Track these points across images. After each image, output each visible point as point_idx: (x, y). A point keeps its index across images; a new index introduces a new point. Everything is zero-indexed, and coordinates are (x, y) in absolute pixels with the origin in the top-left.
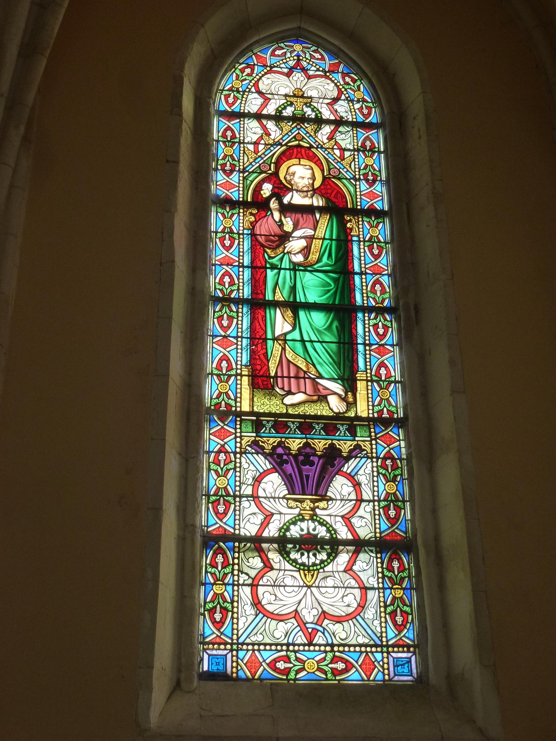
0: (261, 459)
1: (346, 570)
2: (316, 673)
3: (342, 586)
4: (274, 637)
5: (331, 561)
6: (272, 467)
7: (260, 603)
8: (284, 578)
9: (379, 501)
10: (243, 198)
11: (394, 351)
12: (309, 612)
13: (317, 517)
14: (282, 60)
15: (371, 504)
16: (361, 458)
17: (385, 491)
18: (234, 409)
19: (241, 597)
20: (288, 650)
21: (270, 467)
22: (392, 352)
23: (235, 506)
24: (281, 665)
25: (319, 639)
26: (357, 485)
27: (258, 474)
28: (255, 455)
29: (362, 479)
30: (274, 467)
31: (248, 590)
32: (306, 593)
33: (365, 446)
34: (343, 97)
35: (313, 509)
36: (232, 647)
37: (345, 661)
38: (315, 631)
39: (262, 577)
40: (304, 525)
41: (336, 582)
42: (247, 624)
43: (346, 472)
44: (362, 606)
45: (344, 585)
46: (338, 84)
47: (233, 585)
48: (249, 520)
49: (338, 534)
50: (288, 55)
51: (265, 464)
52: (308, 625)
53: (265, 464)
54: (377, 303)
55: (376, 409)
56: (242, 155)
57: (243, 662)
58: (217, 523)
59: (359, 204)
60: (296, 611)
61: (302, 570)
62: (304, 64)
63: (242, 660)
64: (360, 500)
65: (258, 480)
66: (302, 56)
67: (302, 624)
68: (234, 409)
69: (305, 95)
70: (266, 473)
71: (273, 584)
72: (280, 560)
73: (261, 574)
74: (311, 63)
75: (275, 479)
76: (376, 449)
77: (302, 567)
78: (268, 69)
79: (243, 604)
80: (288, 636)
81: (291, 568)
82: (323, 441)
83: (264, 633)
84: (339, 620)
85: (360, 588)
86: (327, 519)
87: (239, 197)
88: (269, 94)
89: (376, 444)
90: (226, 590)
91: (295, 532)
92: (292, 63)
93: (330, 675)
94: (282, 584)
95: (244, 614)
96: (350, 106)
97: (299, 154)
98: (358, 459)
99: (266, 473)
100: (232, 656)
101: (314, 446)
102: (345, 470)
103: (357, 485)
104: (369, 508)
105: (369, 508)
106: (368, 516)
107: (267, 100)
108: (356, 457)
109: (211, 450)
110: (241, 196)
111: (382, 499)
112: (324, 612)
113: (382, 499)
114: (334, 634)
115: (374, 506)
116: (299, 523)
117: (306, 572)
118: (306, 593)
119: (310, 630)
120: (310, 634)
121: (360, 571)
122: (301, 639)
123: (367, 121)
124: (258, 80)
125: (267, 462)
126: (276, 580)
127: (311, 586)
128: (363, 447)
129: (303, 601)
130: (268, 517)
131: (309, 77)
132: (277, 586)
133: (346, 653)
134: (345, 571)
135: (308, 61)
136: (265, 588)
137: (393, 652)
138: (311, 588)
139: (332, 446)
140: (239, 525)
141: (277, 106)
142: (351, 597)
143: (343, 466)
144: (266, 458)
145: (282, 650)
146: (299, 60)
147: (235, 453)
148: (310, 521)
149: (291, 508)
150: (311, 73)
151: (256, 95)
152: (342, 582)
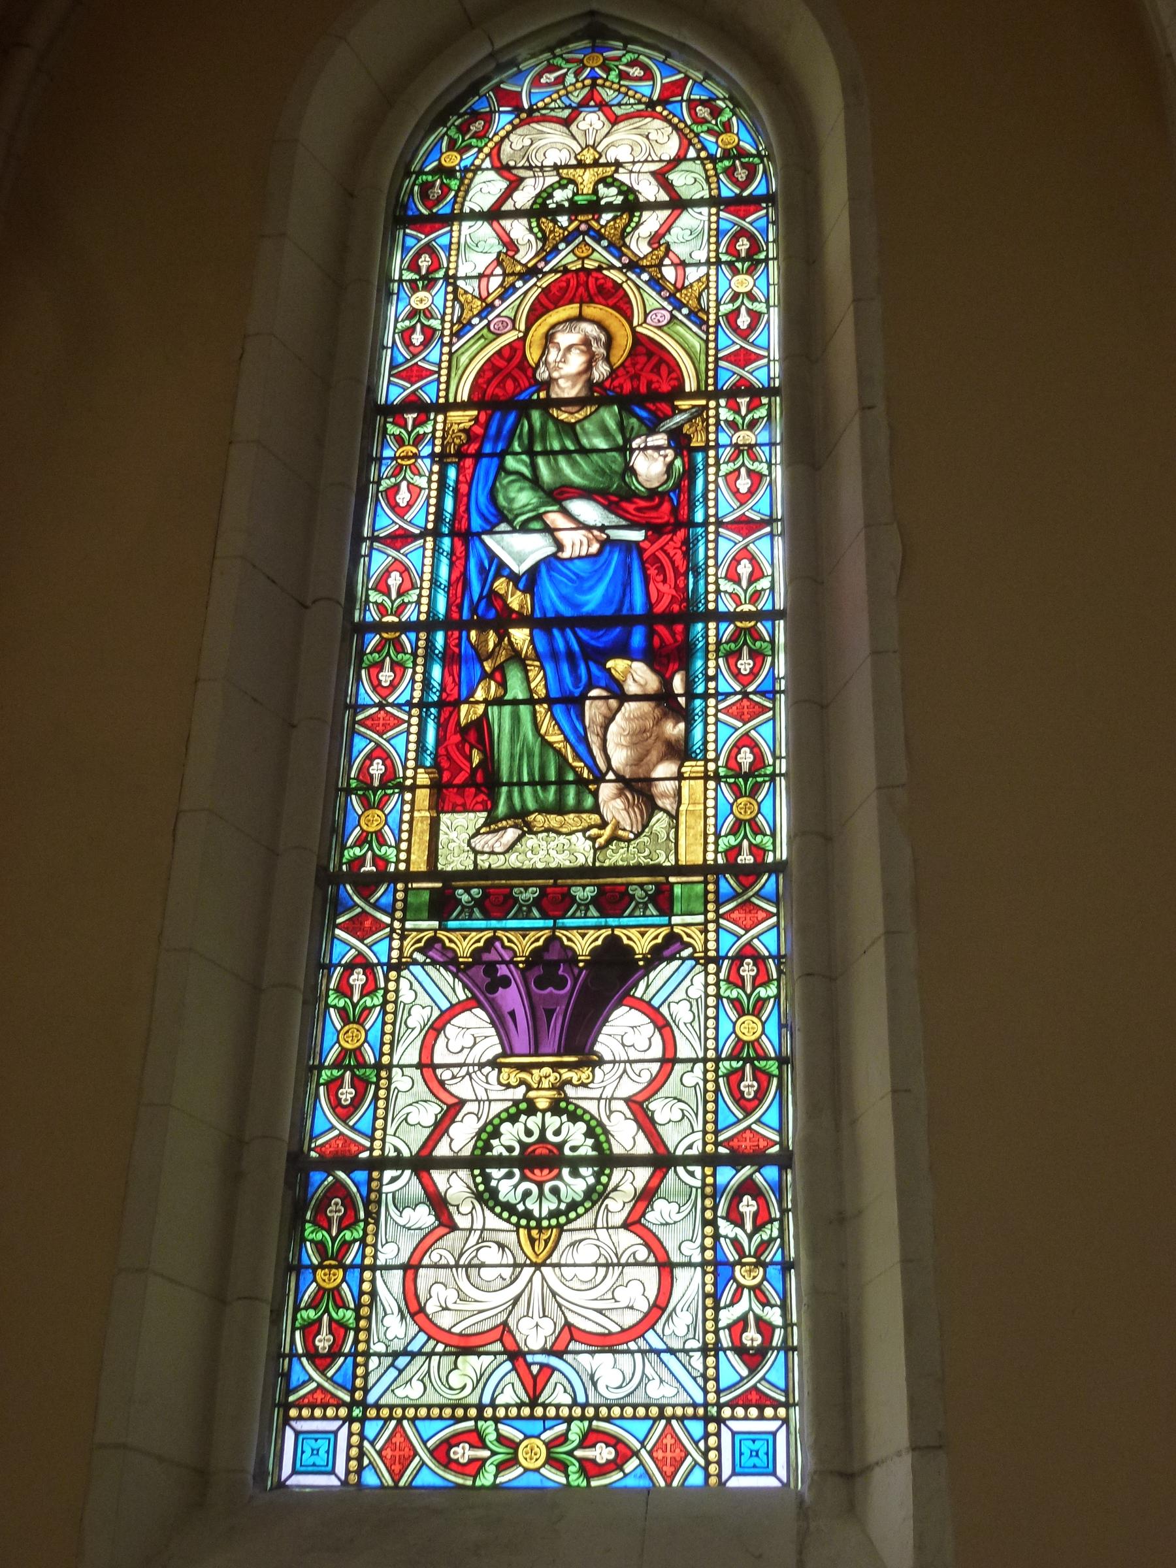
0: (444, 977)
1: (629, 1221)
2: (543, 1471)
3: (615, 1261)
4: (451, 1388)
5: (491, 1123)
6: (470, 995)
7: (422, 1310)
8: (478, 1250)
9: (718, 1060)
10: (447, 397)
11: (774, 709)
12: (537, 1325)
13: (568, 1103)
14: (557, 92)
15: (699, 1067)
16: (684, 960)
17: (733, 1036)
18: (392, 868)
19: (700, 1038)
20: (480, 1417)
21: (462, 997)
22: (770, 709)
23: (378, 1088)
24: (461, 1453)
25: (556, 1395)
26: (663, 1026)
27: (436, 1013)
28: (429, 968)
29: (681, 1013)
30: (474, 996)
31: (684, 1051)
32: (531, 1280)
33: (689, 936)
34: (692, 153)
35: (559, 1087)
36: (350, 1411)
37: (613, 1442)
38: (547, 1371)
39: (652, 1080)
40: (534, 1122)
41: (603, 1252)
42: (687, 982)
43: (641, 999)
44: (659, 1308)
45: (619, 1259)
46: (682, 125)
47: (363, 1268)
48: (406, 1119)
49: (468, 1187)
50: (570, 79)
51: (454, 989)
52: (529, 1358)
53: (454, 989)
54: (739, 603)
55: (724, 843)
56: (449, 304)
57: (374, 1447)
58: (333, 1128)
59: (711, 381)
60: (505, 1324)
61: (524, 1227)
62: (608, 95)
63: (372, 1443)
64: (411, 1268)
65: (436, 1028)
66: (601, 78)
67: (516, 1355)
68: (392, 868)
69: (602, 160)
70: (456, 1009)
71: (452, 1262)
72: (609, 1117)
73: (655, 1085)
74: (623, 89)
75: (476, 1021)
76: (717, 941)
77: (523, 1222)
78: (524, 115)
79: (381, 1313)
80: (481, 1385)
81: (584, 1104)
82: (591, 932)
83: (426, 1380)
84: (607, 1343)
85: (657, 1264)
86: (591, 1106)
87: (438, 397)
88: (523, 167)
89: (717, 932)
90: (344, 1280)
91: (574, 1186)
92: (577, 97)
93: (577, 1475)
94: (475, 1261)
95: (694, 1003)
96: (706, 171)
97: (581, 289)
98: (677, 963)
99: (456, 1009)
100: (350, 1434)
101: (570, 944)
102: (638, 994)
103: (663, 1026)
104: (695, 1076)
105: (695, 1076)
106: (689, 1096)
107: (515, 184)
108: (671, 958)
109: (335, 961)
110: (442, 394)
111: (723, 1056)
112: (568, 1325)
113: (723, 1056)
114: (592, 1377)
115: (706, 1071)
116: (523, 1118)
117: (534, 1233)
118: (531, 1280)
119: (535, 1369)
120: (535, 1378)
121: (425, 1101)
122: (511, 1394)
123: (745, 194)
124: (503, 139)
125: (459, 986)
126: (621, 1077)
127: (544, 1264)
128: (686, 939)
129: (525, 1297)
130: (452, 1110)
131: (615, 121)
132: (620, 1062)
133: (618, 1422)
134: (626, 1225)
135: (616, 86)
136: (648, 1056)
137: (733, 1418)
138: (543, 1269)
139: (613, 942)
140: (384, 1129)
141: (538, 190)
142: (636, 1287)
143: (636, 985)
144: (455, 976)
145: (465, 1418)
146: (594, 85)
147: (391, 967)
148: (548, 1114)
149: (508, 1086)
150: (619, 111)
151: (492, 175)
152: (616, 1255)
